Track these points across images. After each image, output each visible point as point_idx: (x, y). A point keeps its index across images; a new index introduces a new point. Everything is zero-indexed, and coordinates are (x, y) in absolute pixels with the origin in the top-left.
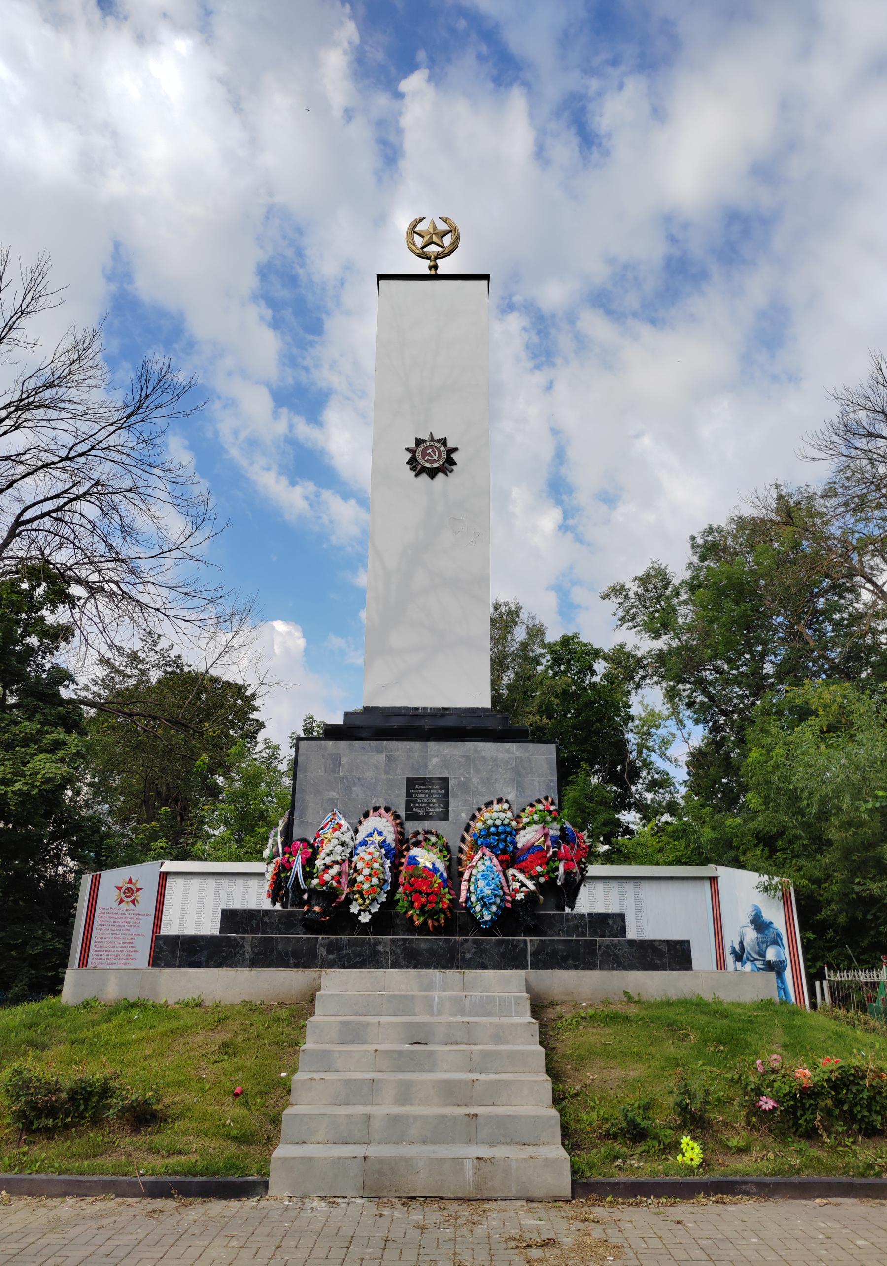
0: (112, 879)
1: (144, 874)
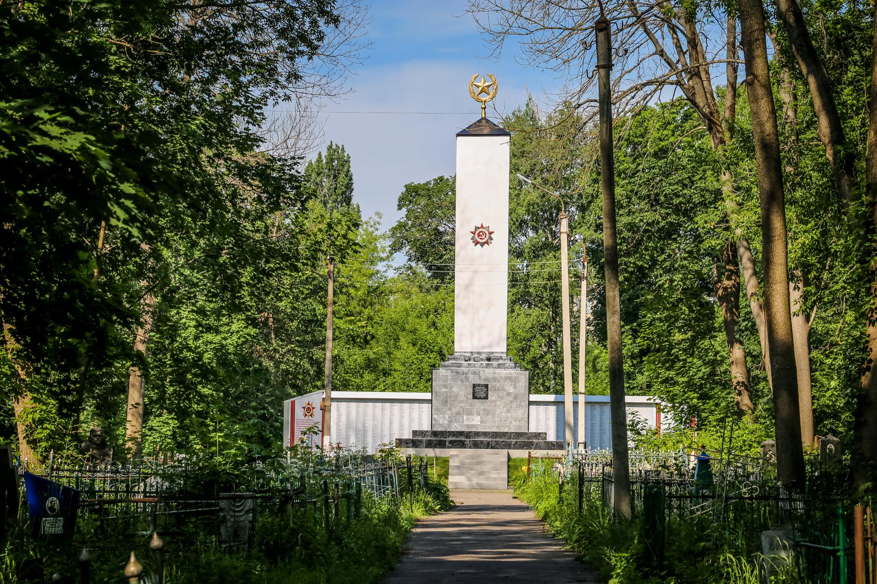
0: (301, 402)
1: (316, 398)
